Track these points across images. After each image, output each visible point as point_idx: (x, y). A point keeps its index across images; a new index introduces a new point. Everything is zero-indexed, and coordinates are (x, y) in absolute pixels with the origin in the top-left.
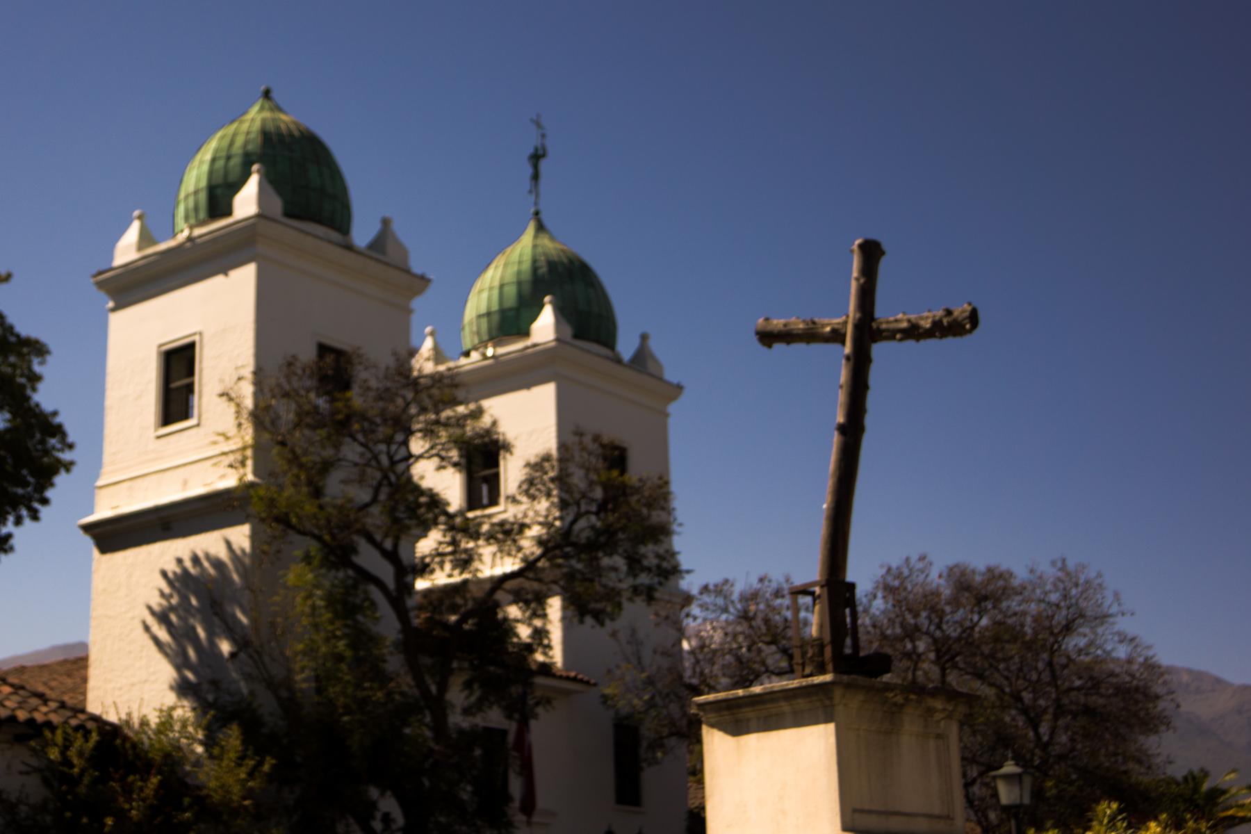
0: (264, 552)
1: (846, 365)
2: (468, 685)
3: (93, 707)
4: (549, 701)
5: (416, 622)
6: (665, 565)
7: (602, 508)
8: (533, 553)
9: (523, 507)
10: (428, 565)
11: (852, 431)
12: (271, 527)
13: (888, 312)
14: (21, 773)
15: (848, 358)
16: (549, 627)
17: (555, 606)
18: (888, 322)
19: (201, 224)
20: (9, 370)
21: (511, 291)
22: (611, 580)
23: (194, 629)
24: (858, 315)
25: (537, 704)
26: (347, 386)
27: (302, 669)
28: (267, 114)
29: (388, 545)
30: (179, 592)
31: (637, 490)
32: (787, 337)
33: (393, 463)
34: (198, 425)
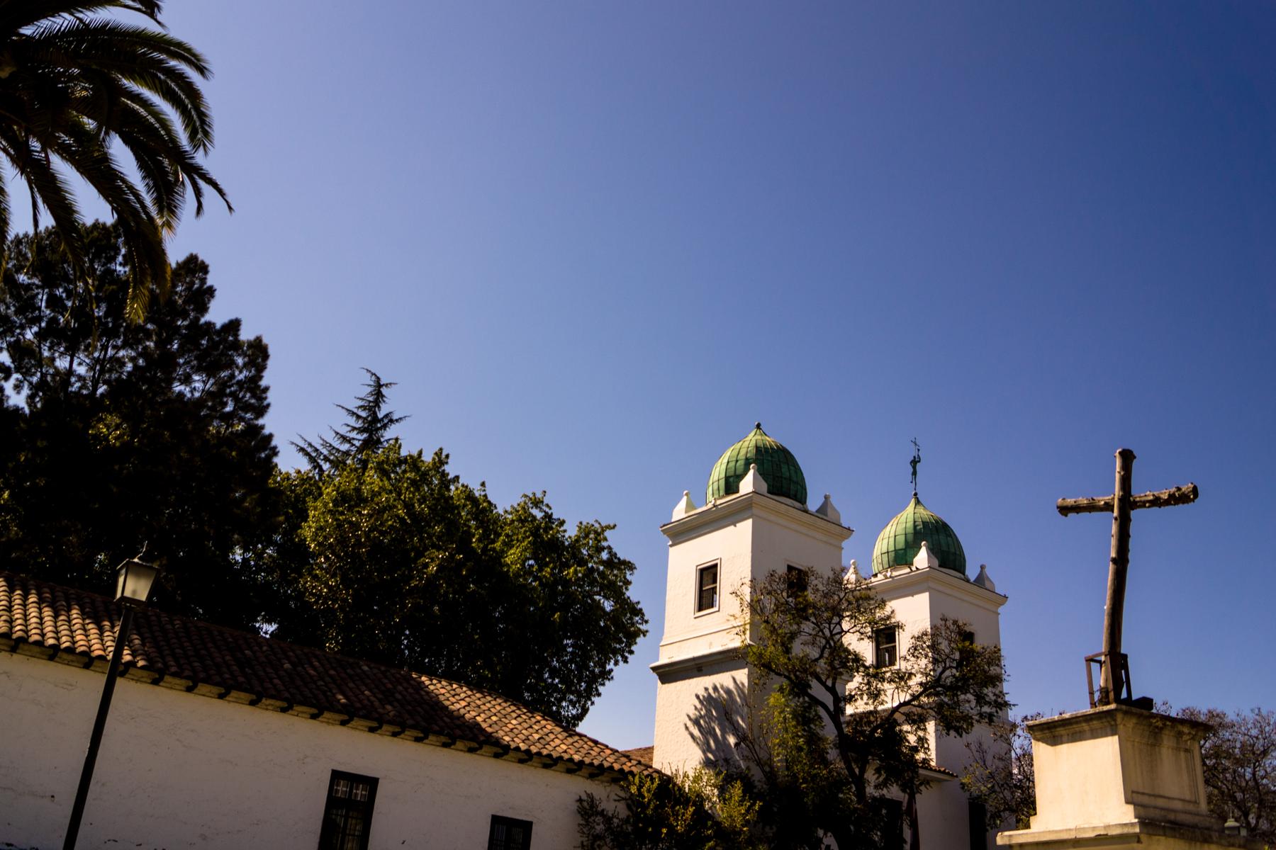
0: (756, 684)
1: (1115, 523)
2: (878, 771)
3: (656, 765)
4: (928, 783)
5: (846, 730)
6: (999, 700)
7: (959, 665)
8: (917, 691)
9: (910, 663)
10: (854, 696)
11: (1121, 562)
12: (760, 669)
13: (1141, 492)
14: (615, 800)
15: (1116, 519)
16: (928, 737)
17: (931, 726)
18: (1140, 497)
19: (723, 497)
20: (614, 578)
21: (901, 539)
22: (966, 708)
23: (714, 729)
24: (1121, 493)
25: (921, 784)
26: (805, 589)
27: (778, 755)
28: (759, 437)
29: (829, 683)
30: (705, 707)
31: (980, 654)
32: (1077, 509)
33: (832, 635)
34: (719, 611)
